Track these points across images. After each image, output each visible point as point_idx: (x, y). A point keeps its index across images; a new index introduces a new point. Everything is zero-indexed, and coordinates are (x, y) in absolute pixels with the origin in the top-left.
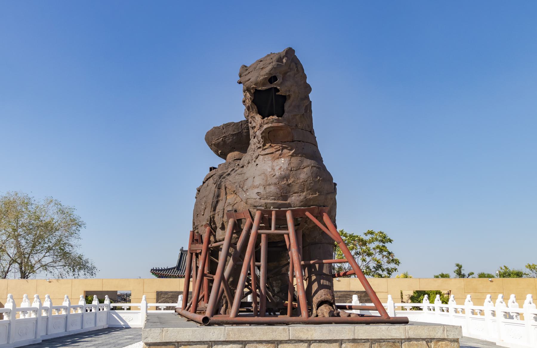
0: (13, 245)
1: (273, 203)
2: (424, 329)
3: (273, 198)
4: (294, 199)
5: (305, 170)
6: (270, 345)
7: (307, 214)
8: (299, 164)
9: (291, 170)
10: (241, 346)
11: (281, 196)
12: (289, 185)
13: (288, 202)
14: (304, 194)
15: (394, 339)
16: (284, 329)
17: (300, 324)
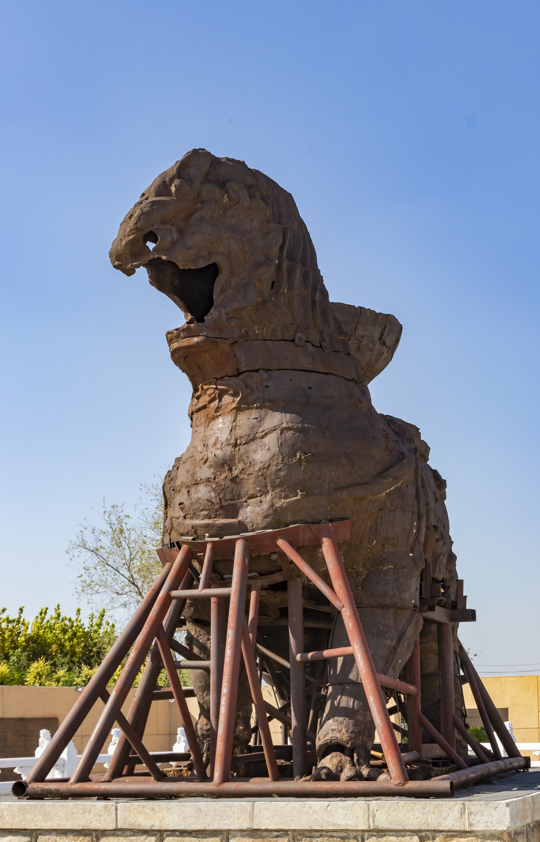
0: (41, 632)
1: (207, 526)
2: (412, 809)
3: (205, 513)
4: (252, 512)
5: (266, 440)
6: (81, 838)
7: (281, 543)
8: (253, 428)
9: (236, 445)
10: (27, 839)
11: (222, 507)
12: (234, 480)
13: (240, 518)
14: (269, 497)
15: (346, 831)
16: (106, 807)
17: (202, 796)
